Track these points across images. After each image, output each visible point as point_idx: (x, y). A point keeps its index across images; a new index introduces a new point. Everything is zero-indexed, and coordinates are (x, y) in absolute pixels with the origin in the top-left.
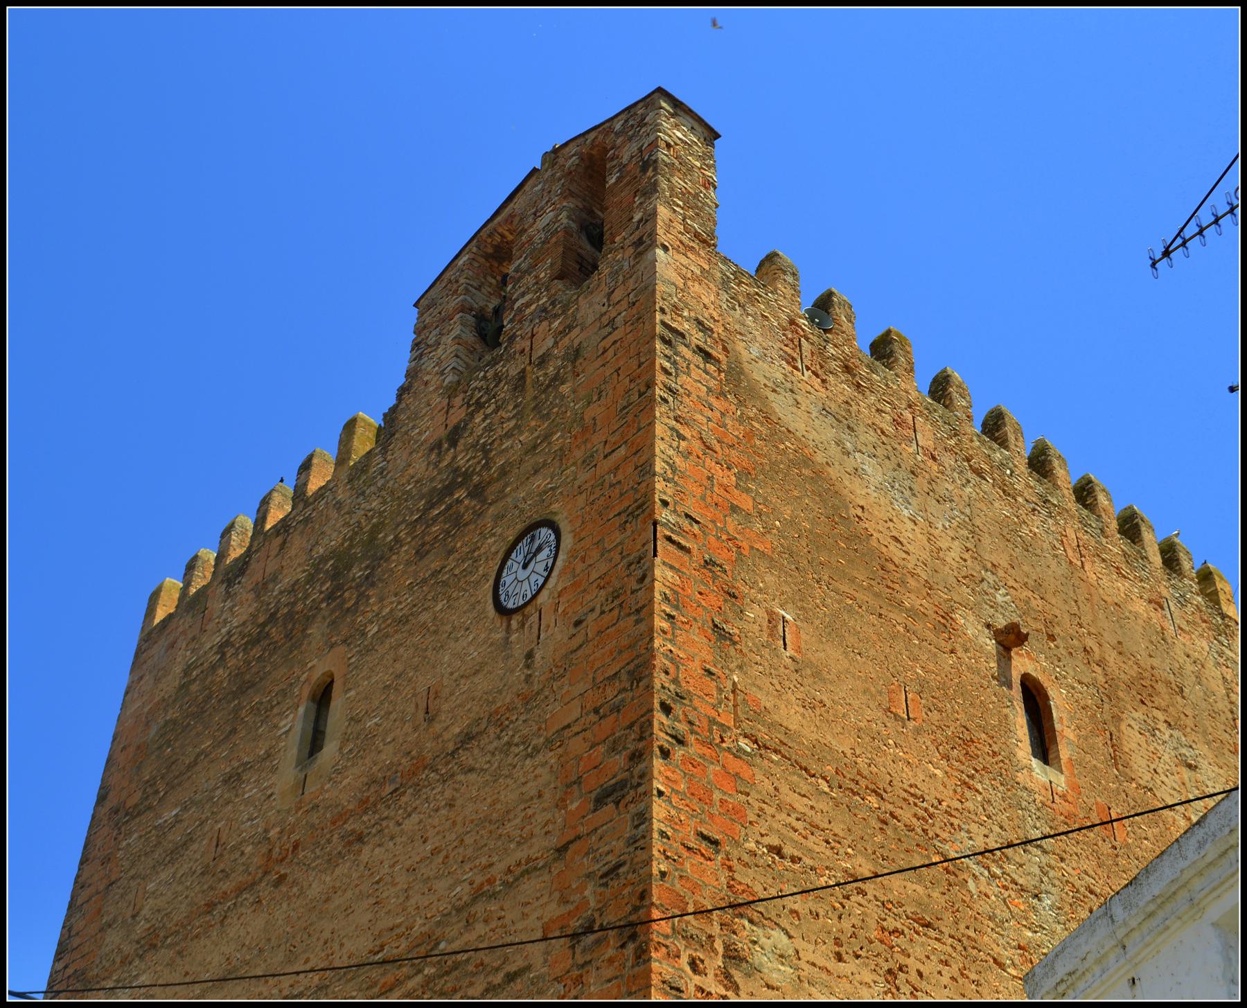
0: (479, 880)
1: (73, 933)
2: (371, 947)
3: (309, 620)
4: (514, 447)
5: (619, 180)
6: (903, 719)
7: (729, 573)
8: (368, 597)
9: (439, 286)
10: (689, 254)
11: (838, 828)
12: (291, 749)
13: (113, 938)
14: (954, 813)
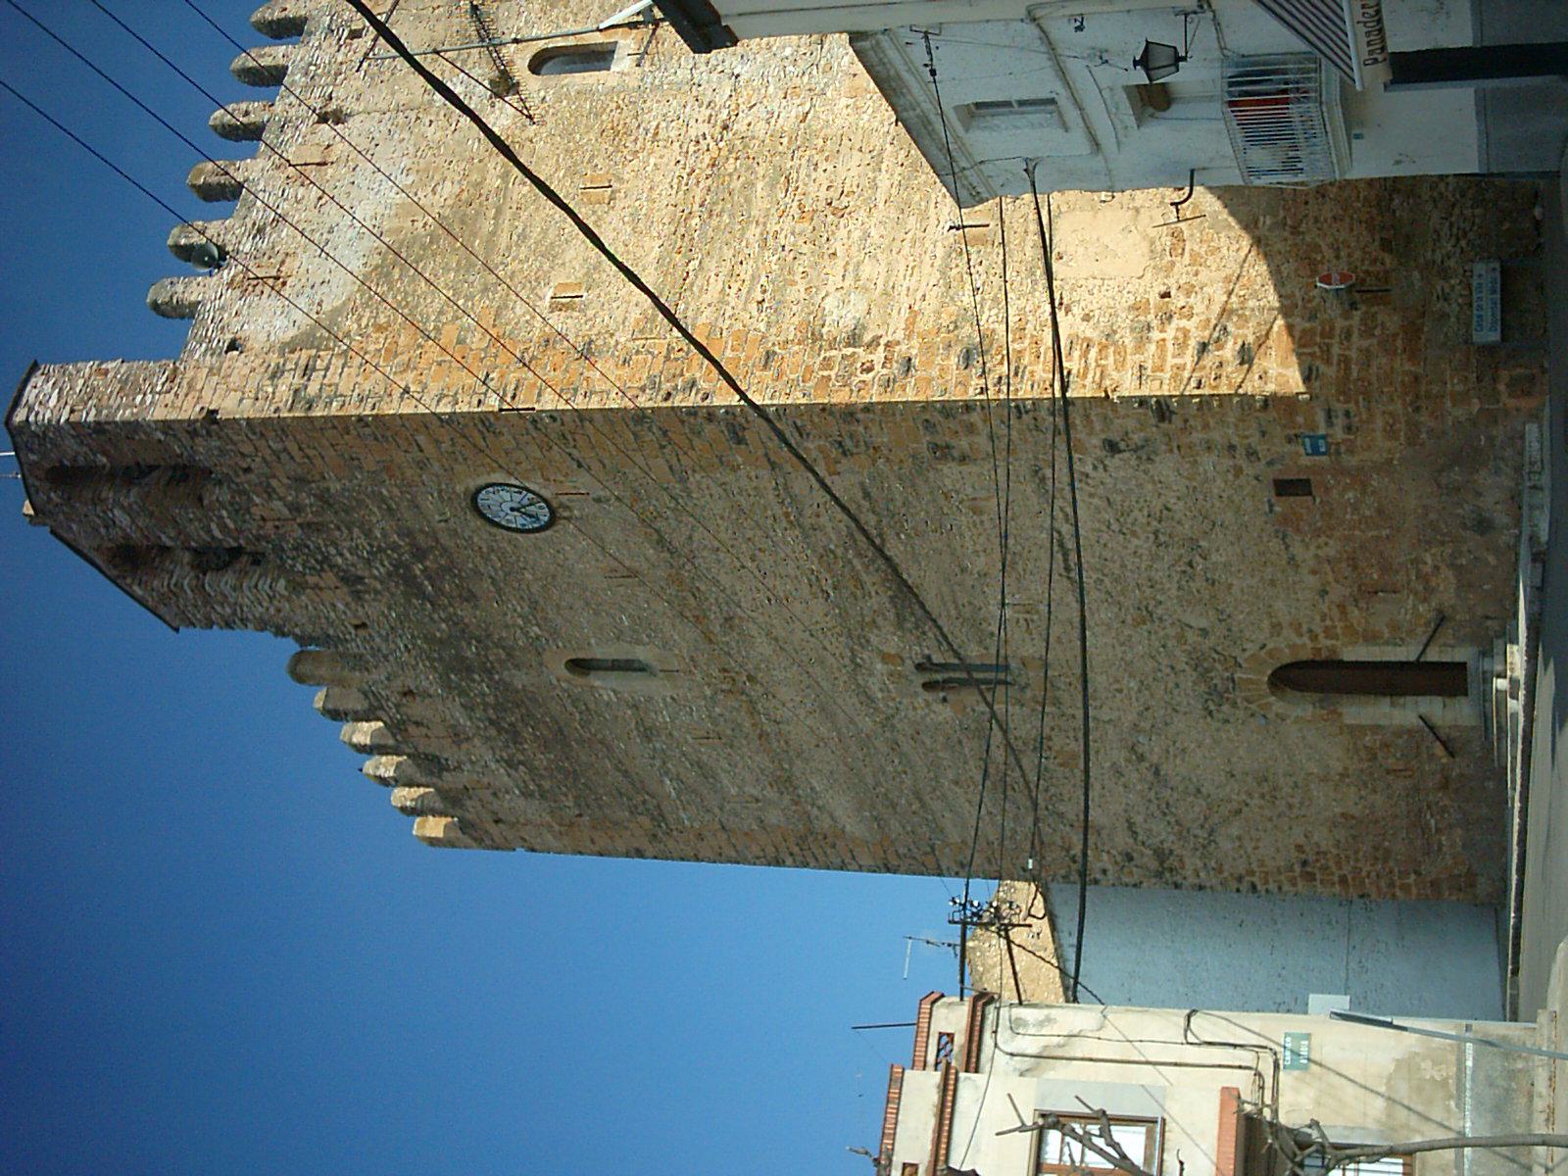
0: (785, 524)
1: (761, 854)
2: (822, 601)
3: (507, 686)
4: (381, 525)
5: (105, 453)
6: (612, 192)
7: (527, 346)
8: (501, 638)
9: (162, 610)
10: (199, 387)
11: (728, 253)
12: (634, 686)
13: (773, 817)
14: (685, 150)
